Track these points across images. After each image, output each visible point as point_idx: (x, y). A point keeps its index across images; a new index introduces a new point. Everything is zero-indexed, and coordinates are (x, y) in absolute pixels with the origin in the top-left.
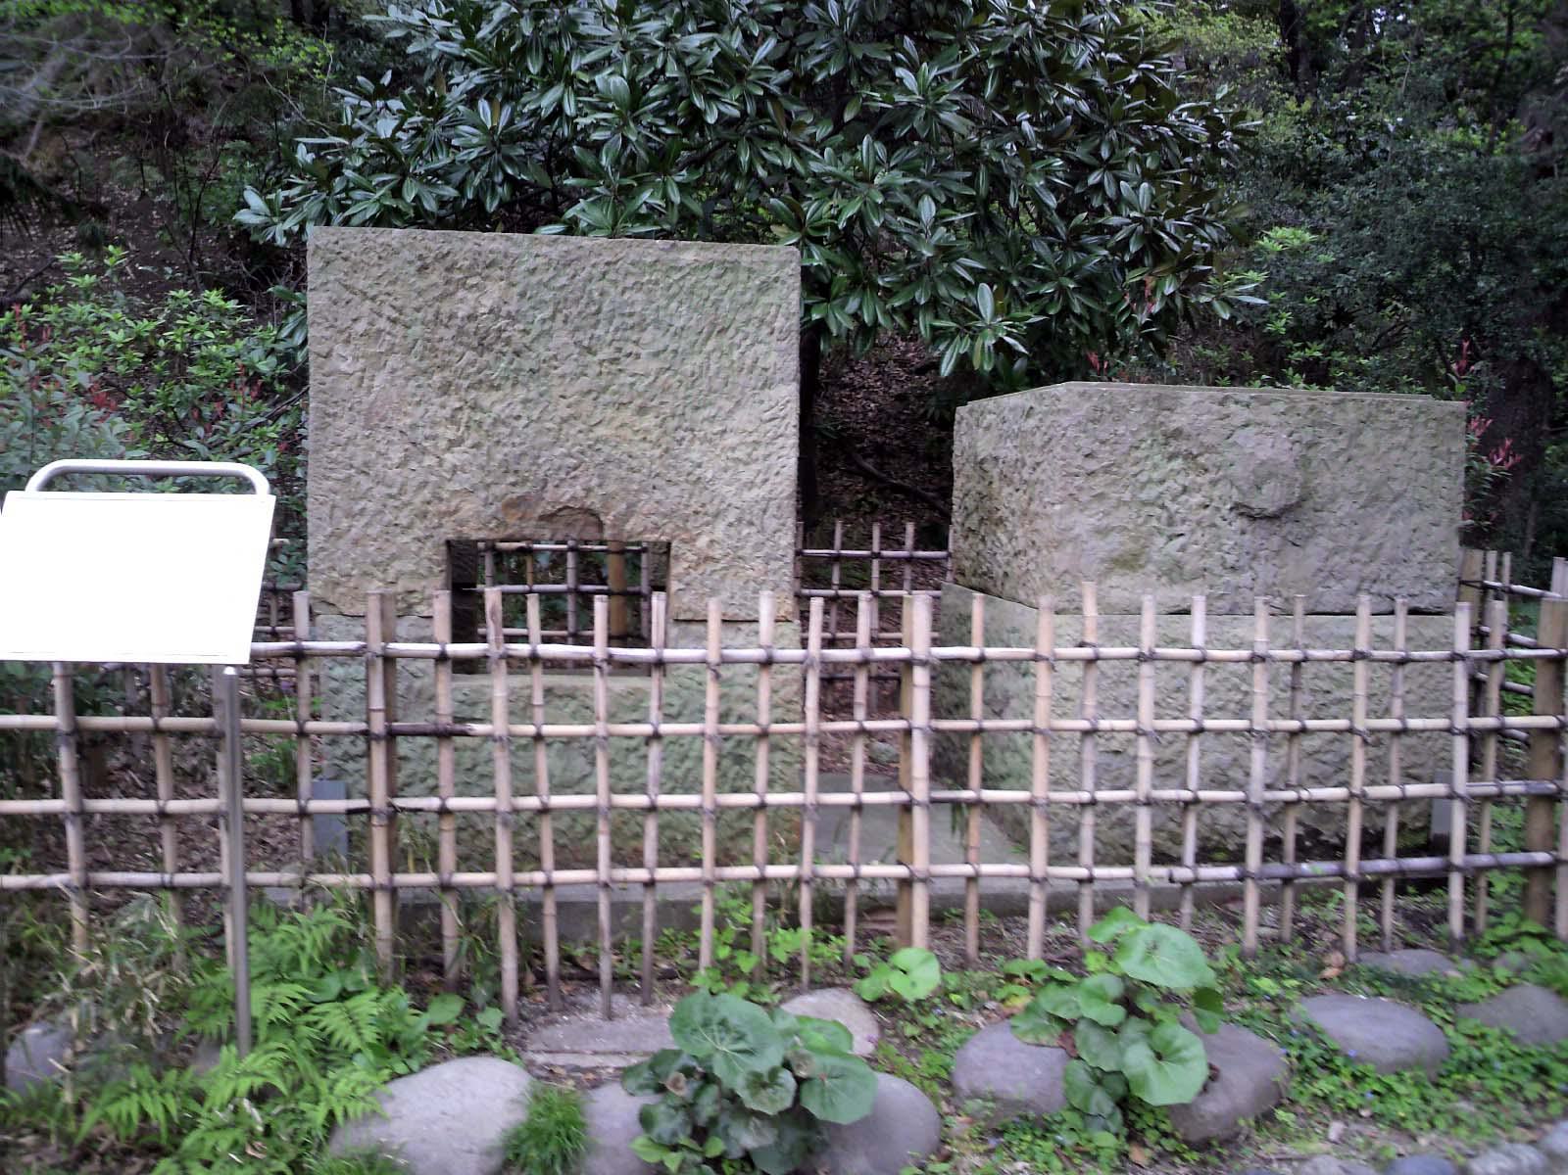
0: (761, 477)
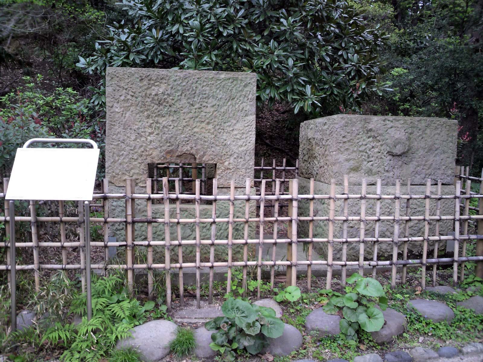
0: (244, 144)
